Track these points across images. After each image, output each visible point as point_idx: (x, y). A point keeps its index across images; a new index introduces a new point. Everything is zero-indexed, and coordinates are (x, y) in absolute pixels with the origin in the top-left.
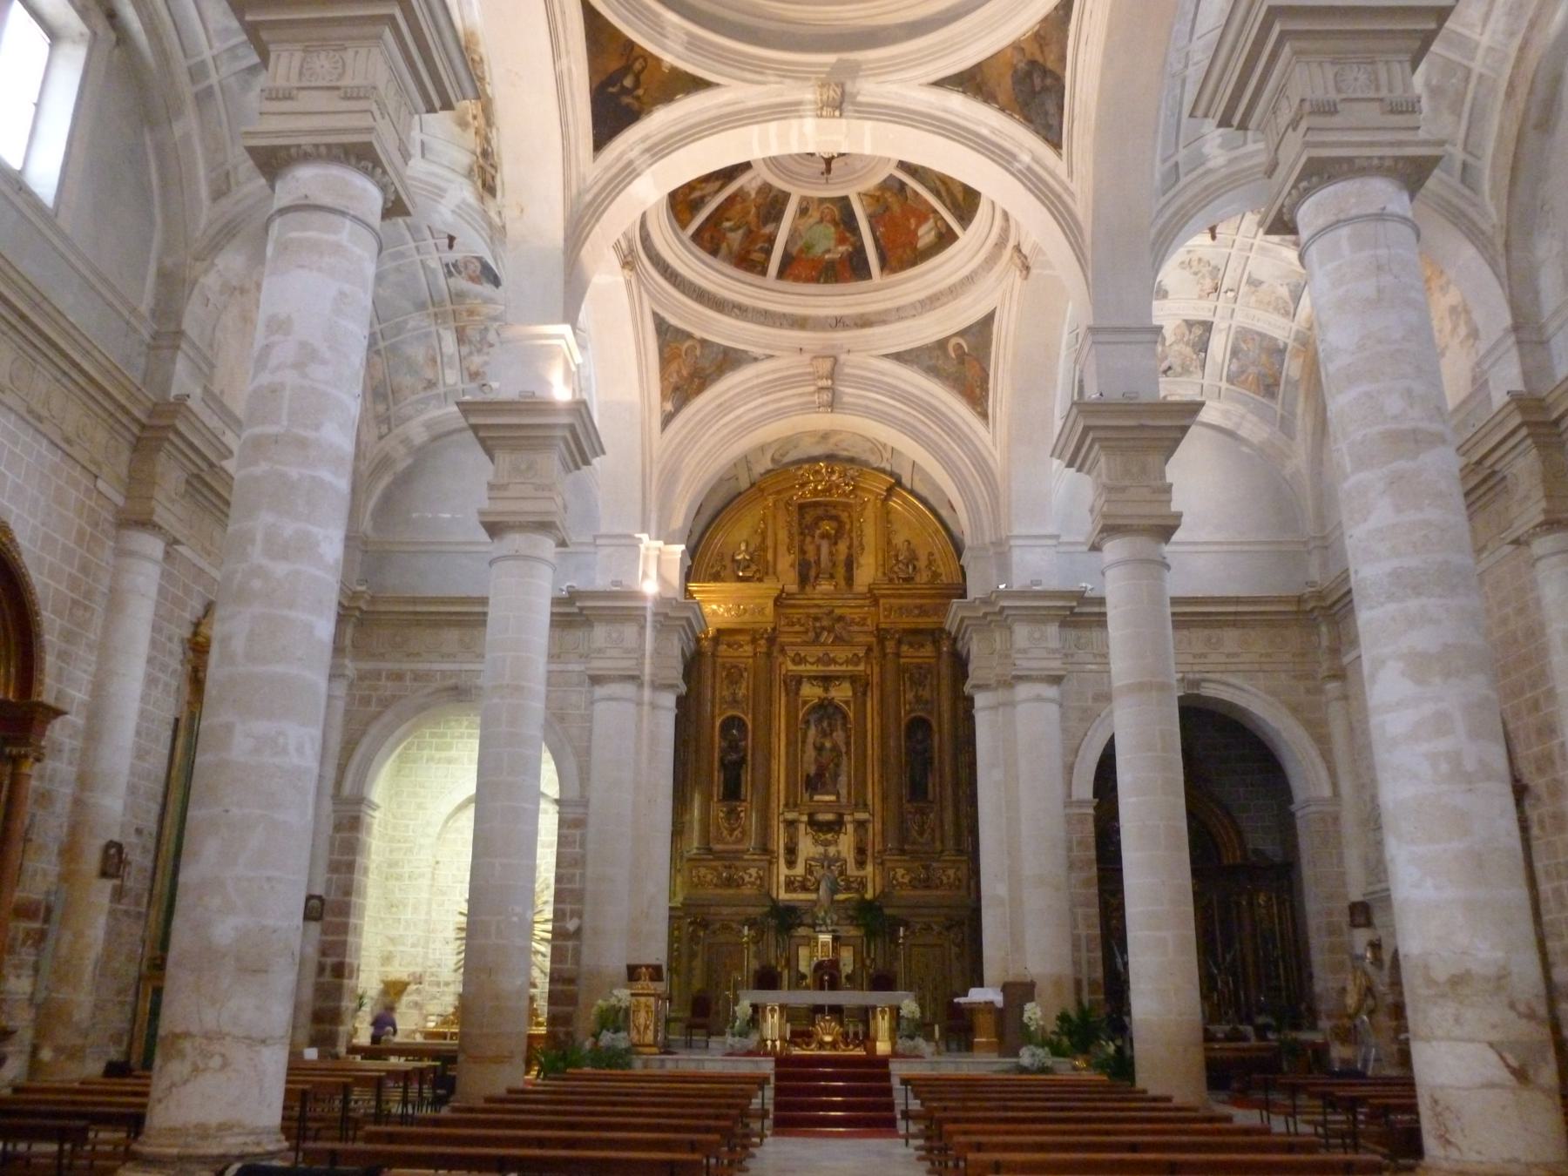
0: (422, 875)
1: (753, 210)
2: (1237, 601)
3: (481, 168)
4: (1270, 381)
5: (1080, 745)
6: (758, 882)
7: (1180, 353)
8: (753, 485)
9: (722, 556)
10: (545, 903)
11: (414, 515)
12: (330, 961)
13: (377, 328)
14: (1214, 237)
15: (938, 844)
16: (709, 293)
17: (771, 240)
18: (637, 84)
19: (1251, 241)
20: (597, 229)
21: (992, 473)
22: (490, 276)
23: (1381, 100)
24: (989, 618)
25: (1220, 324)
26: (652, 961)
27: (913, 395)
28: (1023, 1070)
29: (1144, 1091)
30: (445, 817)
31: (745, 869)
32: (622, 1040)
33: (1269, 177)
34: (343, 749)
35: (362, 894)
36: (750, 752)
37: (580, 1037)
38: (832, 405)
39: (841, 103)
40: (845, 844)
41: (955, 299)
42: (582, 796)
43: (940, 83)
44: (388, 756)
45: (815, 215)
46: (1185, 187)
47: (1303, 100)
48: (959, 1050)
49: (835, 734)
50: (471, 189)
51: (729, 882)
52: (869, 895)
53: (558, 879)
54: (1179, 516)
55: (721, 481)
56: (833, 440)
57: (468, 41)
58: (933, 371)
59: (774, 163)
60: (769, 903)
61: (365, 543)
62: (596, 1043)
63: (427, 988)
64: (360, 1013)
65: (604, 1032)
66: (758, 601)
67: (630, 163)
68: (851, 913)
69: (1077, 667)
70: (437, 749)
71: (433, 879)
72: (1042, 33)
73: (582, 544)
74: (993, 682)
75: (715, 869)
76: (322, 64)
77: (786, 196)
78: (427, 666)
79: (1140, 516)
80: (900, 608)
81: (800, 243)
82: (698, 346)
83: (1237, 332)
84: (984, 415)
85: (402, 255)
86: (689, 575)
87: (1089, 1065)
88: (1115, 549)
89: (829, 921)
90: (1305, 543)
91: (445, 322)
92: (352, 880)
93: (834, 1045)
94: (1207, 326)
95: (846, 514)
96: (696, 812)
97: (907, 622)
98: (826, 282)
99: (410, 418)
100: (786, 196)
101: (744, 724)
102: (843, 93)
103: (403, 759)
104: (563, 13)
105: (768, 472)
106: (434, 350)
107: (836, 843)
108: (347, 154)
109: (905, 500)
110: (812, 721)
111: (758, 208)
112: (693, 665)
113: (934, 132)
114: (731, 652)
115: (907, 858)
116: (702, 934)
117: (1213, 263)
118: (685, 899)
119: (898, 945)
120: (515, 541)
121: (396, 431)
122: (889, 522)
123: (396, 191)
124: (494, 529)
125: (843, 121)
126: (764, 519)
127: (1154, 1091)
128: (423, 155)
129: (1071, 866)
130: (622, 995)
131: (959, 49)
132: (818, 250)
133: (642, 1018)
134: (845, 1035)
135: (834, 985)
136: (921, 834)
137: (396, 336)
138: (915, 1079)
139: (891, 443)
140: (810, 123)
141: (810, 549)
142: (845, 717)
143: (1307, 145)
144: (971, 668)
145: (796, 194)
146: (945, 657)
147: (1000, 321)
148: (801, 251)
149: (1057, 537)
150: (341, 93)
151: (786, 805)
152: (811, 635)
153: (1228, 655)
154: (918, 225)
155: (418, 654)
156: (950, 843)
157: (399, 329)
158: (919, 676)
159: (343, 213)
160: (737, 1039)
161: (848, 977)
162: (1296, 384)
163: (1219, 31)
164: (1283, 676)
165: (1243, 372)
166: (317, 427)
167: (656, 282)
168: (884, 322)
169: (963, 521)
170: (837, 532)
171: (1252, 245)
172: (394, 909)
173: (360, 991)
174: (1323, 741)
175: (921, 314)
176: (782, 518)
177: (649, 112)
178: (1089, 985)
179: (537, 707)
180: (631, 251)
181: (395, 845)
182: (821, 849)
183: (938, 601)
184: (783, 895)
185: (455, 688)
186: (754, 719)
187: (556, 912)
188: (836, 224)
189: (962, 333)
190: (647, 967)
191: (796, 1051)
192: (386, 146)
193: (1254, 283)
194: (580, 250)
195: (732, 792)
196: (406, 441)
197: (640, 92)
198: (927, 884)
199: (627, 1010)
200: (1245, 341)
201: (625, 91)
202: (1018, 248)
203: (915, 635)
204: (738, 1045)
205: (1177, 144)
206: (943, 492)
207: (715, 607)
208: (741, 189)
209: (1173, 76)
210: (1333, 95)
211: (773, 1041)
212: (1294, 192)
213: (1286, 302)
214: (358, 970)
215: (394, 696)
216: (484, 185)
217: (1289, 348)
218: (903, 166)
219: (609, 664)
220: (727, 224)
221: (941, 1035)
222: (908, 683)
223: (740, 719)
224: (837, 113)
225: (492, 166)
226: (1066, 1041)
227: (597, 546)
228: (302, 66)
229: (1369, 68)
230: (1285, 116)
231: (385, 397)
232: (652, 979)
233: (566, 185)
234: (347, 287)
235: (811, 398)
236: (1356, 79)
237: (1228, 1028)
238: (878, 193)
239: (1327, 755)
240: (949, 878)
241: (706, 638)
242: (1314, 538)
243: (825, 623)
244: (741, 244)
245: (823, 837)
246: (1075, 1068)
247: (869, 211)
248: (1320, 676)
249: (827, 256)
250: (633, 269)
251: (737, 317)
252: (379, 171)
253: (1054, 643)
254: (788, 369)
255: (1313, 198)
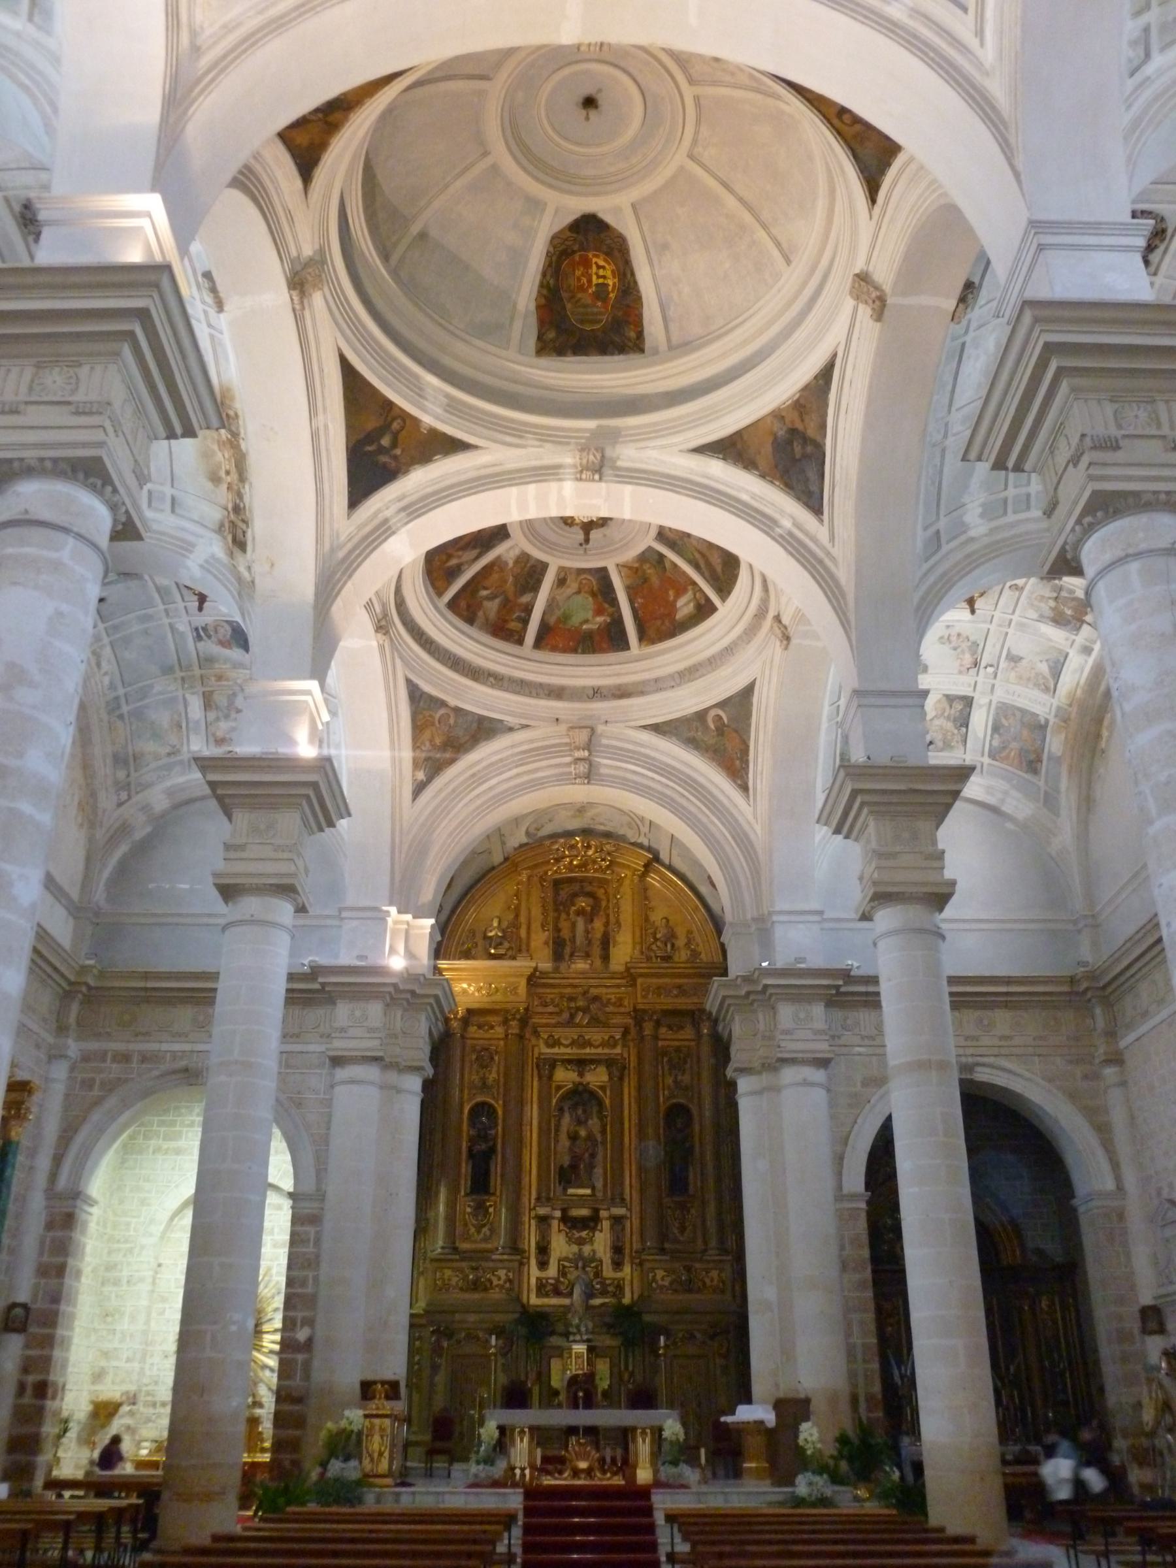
0: (142, 1280)
1: (511, 579)
2: (1008, 981)
3: (232, 522)
4: (1032, 757)
5: (850, 1132)
6: (508, 1285)
7: (942, 728)
8: (506, 859)
9: (473, 933)
10: (276, 1310)
11: (150, 886)
12: (31, 1379)
13: (121, 691)
14: (973, 612)
15: (700, 1242)
16: (464, 661)
17: (528, 609)
18: (394, 444)
19: (1005, 630)
20: (349, 584)
21: (752, 846)
22: (240, 638)
23: (1164, 437)
24: (752, 997)
25: (981, 700)
26: (389, 1376)
27: (674, 768)
28: (799, 1502)
29: (941, 1530)
30: (170, 1214)
31: (494, 1271)
32: (350, 1470)
33: (1049, 516)
34: (61, 1138)
35: (73, 1302)
36: (499, 1141)
37: (307, 1465)
38: (588, 777)
39: (601, 467)
40: (601, 1243)
41: (714, 670)
42: (318, 1190)
43: (700, 450)
44: (109, 1145)
45: (573, 586)
46: (948, 553)
47: (1083, 436)
48: (727, 1477)
49: (590, 1122)
50: (221, 544)
51: (476, 1286)
52: (627, 1300)
53: (290, 1282)
54: (953, 883)
55: (474, 854)
56: (590, 814)
57: (223, 396)
58: (692, 743)
59: (529, 526)
60: (519, 1309)
61: (97, 914)
62: (322, 1475)
63: (142, 1409)
64: (64, 1440)
65: (333, 1461)
66: (512, 980)
67: (386, 521)
68: (607, 1319)
69: (844, 1050)
70: (164, 1139)
71: (154, 1283)
72: (802, 401)
73: (328, 917)
74: (756, 1065)
75: (461, 1270)
76: (55, 380)
77: (544, 566)
78: (153, 1046)
79: (915, 884)
80: (658, 988)
81: (558, 613)
82: (452, 715)
83: (997, 708)
84: (745, 788)
85: (148, 618)
86: (439, 951)
87: (871, 1492)
88: (887, 918)
89: (583, 1329)
90: (1075, 922)
91: (192, 687)
92: (62, 1284)
93: (589, 1472)
94: (968, 702)
95: (602, 891)
96: (441, 1208)
97: (667, 1002)
98: (584, 652)
99: (148, 786)
100: (544, 566)
101: (495, 1111)
102: (603, 456)
103: (126, 1149)
104: (321, 370)
105: (521, 846)
106: (180, 714)
107: (591, 1241)
108: (74, 470)
109: (663, 877)
110: (566, 1108)
111: (516, 577)
112: (441, 1048)
113: (696, 498)
114: (481, 1034)
115: (667, 1258)
116: (445, 1344)
117: (972, 638)
118: (427, 1305)
119: (659, 1356)
120: (251, 905)
121: (136, 798)
122: (646, 898)
123: (127, 512)
124: (228, 892)
125: (603, 485)
126: (517, 895)
127: (955, 1528)
128: (173, 511)
129: (844, 1267)
130: (354, 1417)
131: (718, 418)
132: (575, 621)
133: (375, 1444)
134: (602, 1460)
135: (589, 1403)
136: (683, 1229)
137: (141, 699)
138: (682, 1515)
139: (649, 816)
140: (569, 487)
141: (564, 925)
142: (600, 1103)
143: (1091, 478)
144: (733, 1050)
145: (555, 564)
146: (705, 1039)
147: (761, 693)
148: (559, 620)
149: (821, 913)
150: (72, 408)
151: (538, 1199)
152: (566, 1016)
153: (1002, 1038)
154: (678, 595)
155: (147, 1034)
156: (713, 1243)
157: (144, 693)
158: (678, 1060)
159: (65, 530)
160: (481, 1467)
161: (605, 1394)
162: (1058, 760)
163: (979, 403)
164: (1058, 1060)
165: (1004, 748)
166: (20, 755)
167: (410, 649)
168: (642, 693)
169: (724, 899)
170: (593, 909)
171: (1011, 620)
172: (109, 1319)
173: (65, 1414)
174: (1103, 1130)
175: (679, 685)
176: (536, 894)
177: (406, 472)
178: (867, 1400)
179: (268, 1085)
180: (385, 615)
181: (116, 1246)
182: (575, 1248)
183: (695, 980)
184: (534, 1300)
185: (186, 1070)
186: (505, 1106)
187: (285, 1319)
188: (593, 594)
189: (722, 705)
190: (383, 1383)
191: (548, 1481)
192: (119, 461)
193: (1014, 659)
194: (331, 605)
195: (480, 1184)
196: (146, 808)
197: (398, 452)
198: (688, 1287)
199: (360, 1434)
200: (1006, 717)
201: (382, 450)
202: (778, 619)
203: (675, 1017)
204: (483, 1475)
205: (938, 514)
206: (701, 866)
207: (465, 986)
208: (499, 558)
209: (934, 445)
210: (1113, 431)
211: (523, 1469)
212: (1078, 528)
213: (1044, 677)
214: (64, 1386)
215: (119, 1079)
216: (234, 540)
217: (1051, 723)
218: (663, 535)
219: (352, 1044)
220: (484, 593)
221: (707, 1460)
222: (666, 1068)
223: (490, 1106)
224: (597, 477)
225: (243, 521)
226: (844, 1466)
227: (342, 919)
228: (32, 381)
229: (1149, 407)
230: (1064, 453)
231: (126, 763)
232: (388, 1398)
233: (319, 540)
234: (65, 607)
235: (566, 770)
236: (1136, 416)
237: (1017, 1448)
238: (636, 565)
239: (1108, 1146)
240: (712, 1280)
241: (455, 1018)
242: (1085, 916)
243: (581, 1003)
244: (499, 611)
245: (577, 1235)
246: (857, 1499)
247: (628, 582)
248: (1097, 1061)
249: (584, 627)
250: (386, 633)
251: (492, 686)
252: (109, 489)
253: (820, 1025)
254: (544, 739)
255: (1105, 529)
